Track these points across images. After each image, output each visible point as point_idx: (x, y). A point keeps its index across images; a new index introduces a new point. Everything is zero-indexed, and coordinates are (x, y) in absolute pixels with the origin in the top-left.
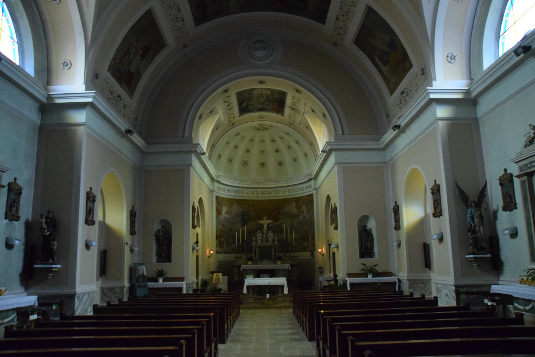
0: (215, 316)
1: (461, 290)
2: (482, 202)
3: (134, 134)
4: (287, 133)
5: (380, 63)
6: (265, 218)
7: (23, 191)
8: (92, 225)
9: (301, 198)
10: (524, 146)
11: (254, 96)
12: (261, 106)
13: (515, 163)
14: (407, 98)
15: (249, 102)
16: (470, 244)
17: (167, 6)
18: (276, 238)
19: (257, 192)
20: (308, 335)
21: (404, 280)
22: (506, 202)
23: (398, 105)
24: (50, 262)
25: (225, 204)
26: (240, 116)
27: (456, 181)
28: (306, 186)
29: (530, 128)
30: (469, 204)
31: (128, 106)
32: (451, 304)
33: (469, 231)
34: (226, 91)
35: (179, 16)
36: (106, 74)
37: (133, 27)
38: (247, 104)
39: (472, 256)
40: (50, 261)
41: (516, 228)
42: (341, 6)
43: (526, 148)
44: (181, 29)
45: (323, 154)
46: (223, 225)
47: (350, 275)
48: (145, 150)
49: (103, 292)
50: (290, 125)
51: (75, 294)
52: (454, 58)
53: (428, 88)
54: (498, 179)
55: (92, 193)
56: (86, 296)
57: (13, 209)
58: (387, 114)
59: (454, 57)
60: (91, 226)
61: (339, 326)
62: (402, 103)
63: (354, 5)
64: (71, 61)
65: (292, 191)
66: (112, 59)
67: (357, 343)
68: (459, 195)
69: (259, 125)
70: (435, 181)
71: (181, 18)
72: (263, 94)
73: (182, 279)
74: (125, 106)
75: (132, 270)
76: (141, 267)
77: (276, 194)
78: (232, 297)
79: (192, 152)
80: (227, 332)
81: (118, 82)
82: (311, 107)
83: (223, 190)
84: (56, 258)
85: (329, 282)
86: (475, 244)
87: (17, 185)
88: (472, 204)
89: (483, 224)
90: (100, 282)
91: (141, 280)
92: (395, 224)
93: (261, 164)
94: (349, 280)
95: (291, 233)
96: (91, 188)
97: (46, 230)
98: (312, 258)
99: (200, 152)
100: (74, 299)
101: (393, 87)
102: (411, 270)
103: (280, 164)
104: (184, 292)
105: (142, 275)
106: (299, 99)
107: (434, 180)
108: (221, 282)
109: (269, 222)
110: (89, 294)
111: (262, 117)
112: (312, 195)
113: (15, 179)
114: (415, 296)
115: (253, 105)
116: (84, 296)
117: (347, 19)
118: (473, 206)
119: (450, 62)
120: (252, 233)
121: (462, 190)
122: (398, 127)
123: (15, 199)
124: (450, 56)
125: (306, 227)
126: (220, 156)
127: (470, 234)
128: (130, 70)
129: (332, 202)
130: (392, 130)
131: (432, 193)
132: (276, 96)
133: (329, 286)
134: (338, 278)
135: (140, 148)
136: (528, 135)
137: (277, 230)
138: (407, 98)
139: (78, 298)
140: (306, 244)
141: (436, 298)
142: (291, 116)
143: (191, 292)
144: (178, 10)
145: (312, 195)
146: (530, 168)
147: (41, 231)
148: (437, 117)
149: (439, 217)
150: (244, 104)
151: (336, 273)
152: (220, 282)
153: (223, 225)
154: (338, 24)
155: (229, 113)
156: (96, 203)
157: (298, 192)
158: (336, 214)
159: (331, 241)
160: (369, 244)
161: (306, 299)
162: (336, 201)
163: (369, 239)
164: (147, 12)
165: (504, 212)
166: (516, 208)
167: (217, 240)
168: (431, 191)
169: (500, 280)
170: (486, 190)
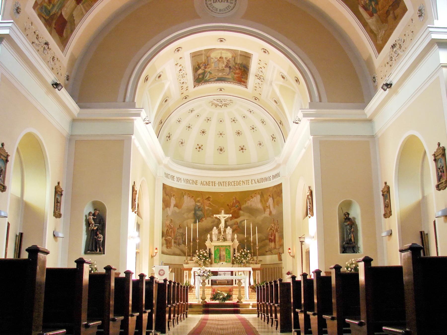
3: (62, 90)
11: (212, 60)
12: (220, 74)
15: (205, 68)
19: (213, 183)
23: (388, 63)
25: (174, 195)
34: (178, 50)
38: (203, 71)
46: (171, 220)
58: (374, 78)
62: (393, 59)
65: (256, 181)
70: (439, 144)
92: (385, 210)
93: (219, 150)
95: (254, 233)
98: (280, 262)
103: (242, 149)
107: (437, 143)
109: (227, 216)
111: (221, 90)
115: (211, 73)
125: (273, 225)
126: (169, 137)
128: (61, 14)
131: (435, 160)
140: (272, 245)
150: (200, 71)
153: (171, 220)
155: (182, 82)
156: (8, 164)
160: (352, 236)
163: (352, 230)
167: (164, 238)
168: (433, 158)
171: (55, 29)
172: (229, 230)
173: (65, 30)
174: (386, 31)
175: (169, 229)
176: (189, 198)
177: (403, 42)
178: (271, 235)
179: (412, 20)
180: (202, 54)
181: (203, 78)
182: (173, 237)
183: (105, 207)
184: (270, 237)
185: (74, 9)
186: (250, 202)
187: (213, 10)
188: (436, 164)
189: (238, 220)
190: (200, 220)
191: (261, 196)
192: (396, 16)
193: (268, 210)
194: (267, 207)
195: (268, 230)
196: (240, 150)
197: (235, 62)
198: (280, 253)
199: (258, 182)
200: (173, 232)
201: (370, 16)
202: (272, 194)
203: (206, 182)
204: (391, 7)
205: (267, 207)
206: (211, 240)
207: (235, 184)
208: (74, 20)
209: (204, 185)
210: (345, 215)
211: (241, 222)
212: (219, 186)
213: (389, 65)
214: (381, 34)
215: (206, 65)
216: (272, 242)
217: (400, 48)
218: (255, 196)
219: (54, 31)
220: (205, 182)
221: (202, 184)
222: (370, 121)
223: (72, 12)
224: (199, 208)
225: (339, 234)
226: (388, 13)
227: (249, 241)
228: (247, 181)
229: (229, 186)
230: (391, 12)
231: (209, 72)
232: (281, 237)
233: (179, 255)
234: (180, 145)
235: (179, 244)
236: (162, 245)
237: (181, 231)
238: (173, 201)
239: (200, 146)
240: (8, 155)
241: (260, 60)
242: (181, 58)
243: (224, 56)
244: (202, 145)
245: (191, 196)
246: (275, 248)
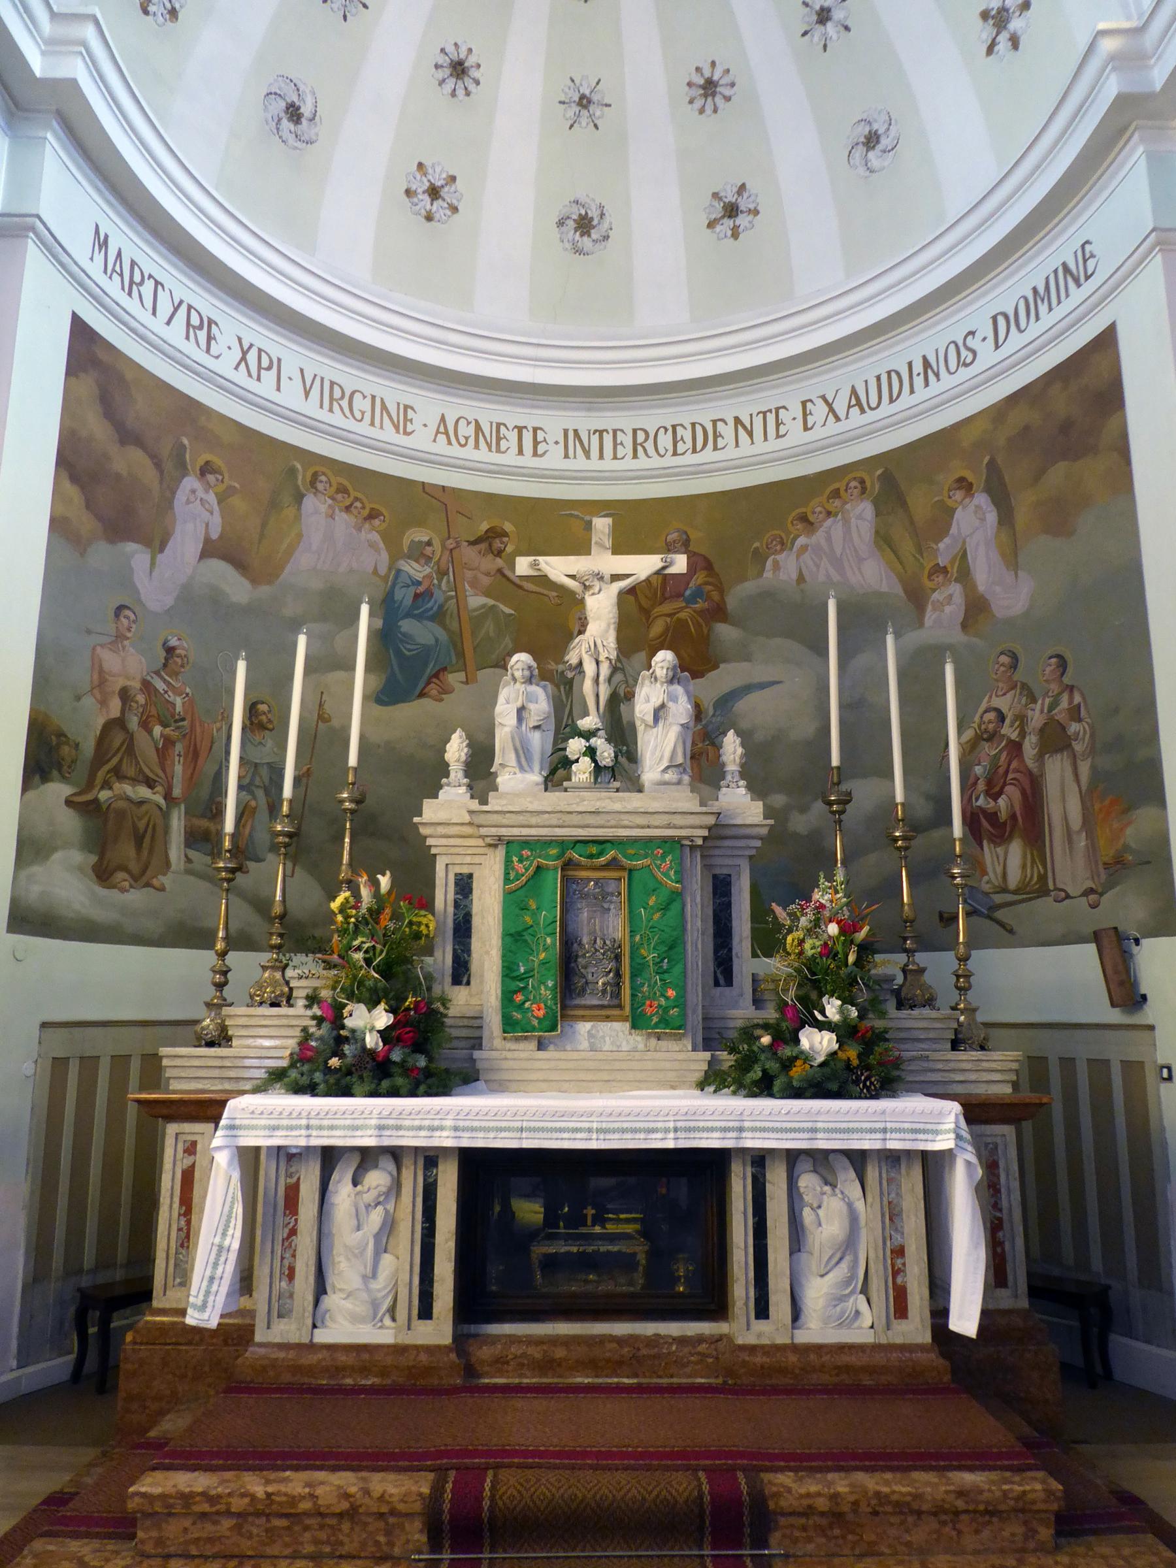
19: (528, 437)
46: (170, 651)
65: (840, 407)
77: (694, 451)
93: (571, 224)
109: (643, 566)
125: (1003, 703)
153: (170, 651)
175: (145, 725)
176: (342, 517)
178: (990, 783)
182: (177, 792)
186: (793, 557)
190: (428, 683)
193: (956, 590)
198: (1119, 936)
199: (855, 411)
200: (179, 747)
202: (992, 466)
203: (478, 428)
205: (944, 570)
207: (680, 444)
209: (462, 446)
212: (566, 456)
218: (829, 514)
220: (469, 423)
221: (447, 433)
224: (417, 596)
228: (771, 418)
229: (635, 456)
234: (280, 120)
245: (358, 504)
246: (1039, 888)
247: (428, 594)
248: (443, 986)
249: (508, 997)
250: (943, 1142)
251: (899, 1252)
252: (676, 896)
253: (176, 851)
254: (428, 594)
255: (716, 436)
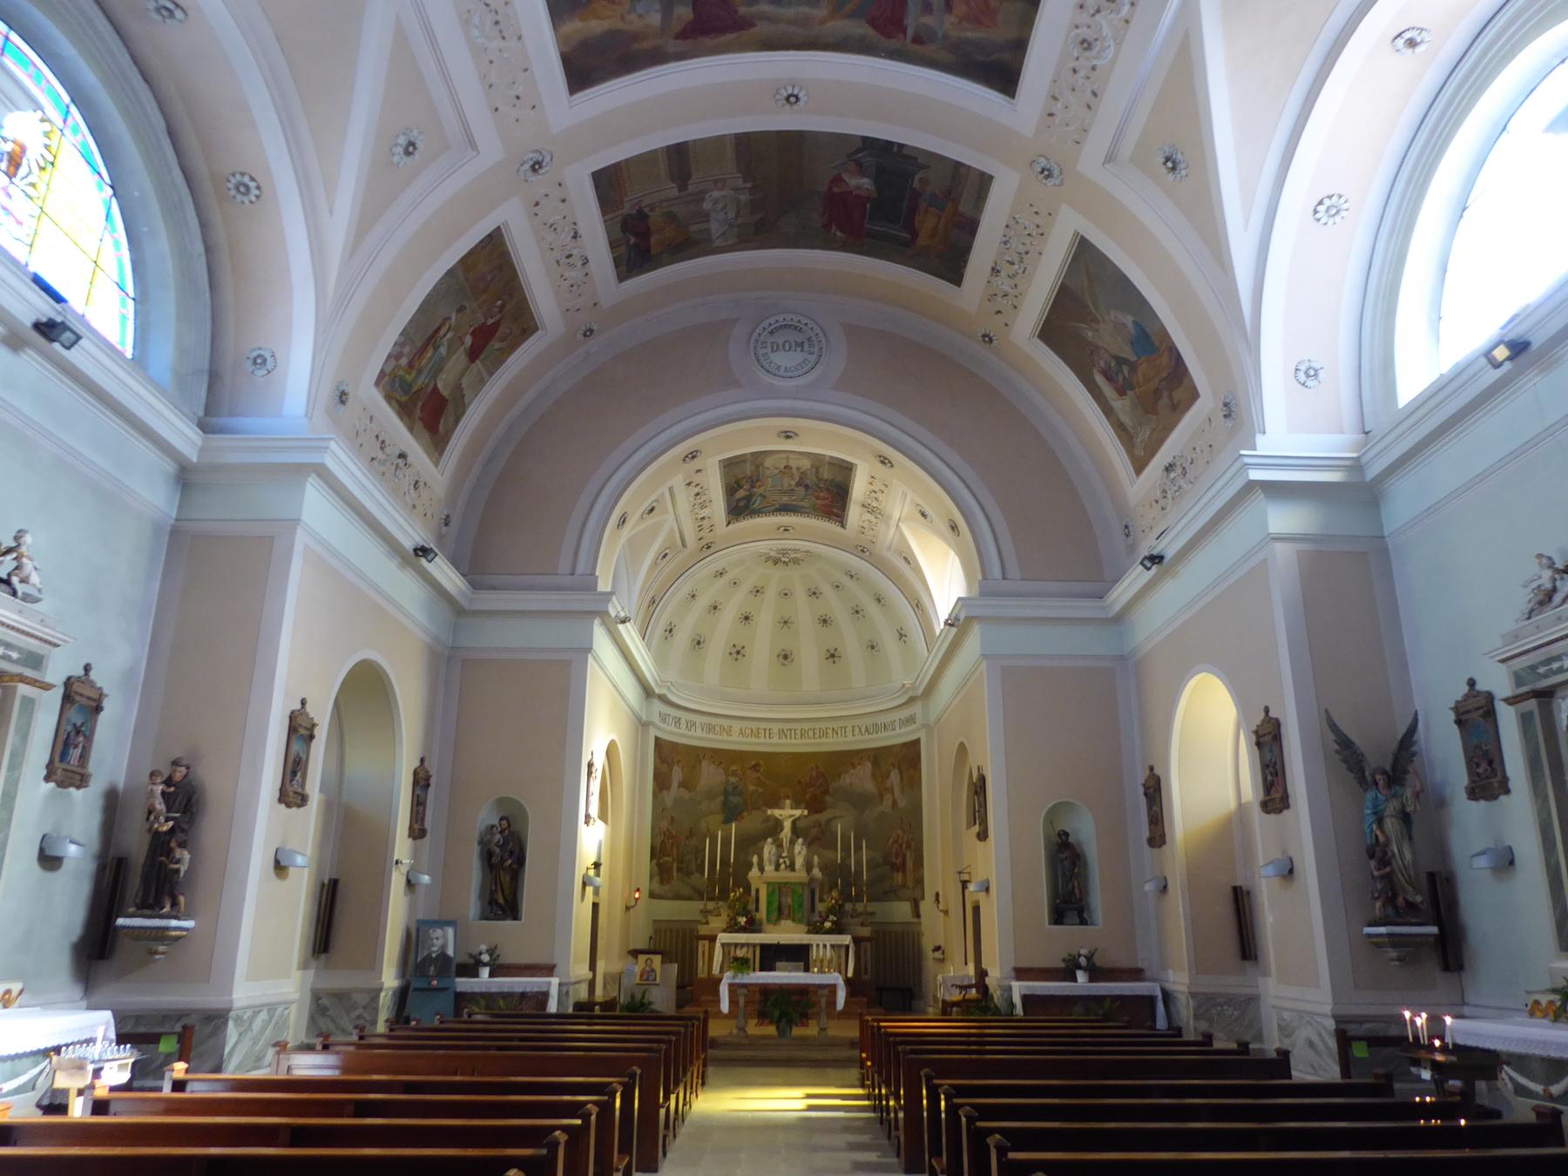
0: (677, 1042)
1: (1353, 1029)
2: (1406, 772)
4: (853, 573)
5: (1108, 391)
6: (788, 802)
7: (106, 703)
8: (299, 806)
9: (886, 750)
10: (1524, 614)
11: (768, 472)
12: (785, 499)
13: (1503, 661)
14: (1182, 483)
15: (753, 487)
16: (1376, 895)
17: (545, 224)
18: (816, 859)
20: (902, 1152)
21: (1182, 993)
22: (1478, 774)
23: (1157, 502)
24: (165, 910)
25: (678, 762)
26: (727, 526)
27: (1326, 711)
28: (900, 719)
29: (1540, 563)
30: (1369, 778)
31: (425, 484)
32: (1326, 1071)
33: (1371, 856)
34: (693, 455)
35: (574, 252)
36: (369, 395)
37: (450, 273)
38: (748, 493)
39: (1382, 930)
40: (163, 908)
41: (1510, 848)
42: (1005, 236)
43: (1530, 621)
44: (579, 286)
45: (948, 631)
47: (1022, 973)
48: (466, 605)
49: (318, 1005)
50: (861, 554)
51: (229, 1010)
52: (1316, 375)
53: (1243, 452)
54: (1452, 709)
55: (307, 714)
56: (263, 1015)
57: (71, 751)
58: (1126, 527)
59: (1316, 371)
60: (294, 809)
61: (1000, 1134)
62: (1169, 496)
63: (1042, 235)
64: (276, 354)
65: (863, 731)
66: (389, 357)
67: (1012, 1155)
68: (1337, 752)
69: (778, 551)
70: (1267, 710)
71: (582, 256)
72: (790, 468)
73: (549, 970)
74: (417, 482)
75: (413, 940)
76: (439, 932)
77: (820, 737)
78: (686, 1027)
79: (593, 614)
80: (665, 1137)
81: (401, 418)
82: (918, 505)
83: (676, 723)
84: (182, 899)
85: (964, 992)
86: (1390, 894)
87: (92, 684)
88: (1378, 777)
89: (1410, 838)
90: (311, 972)
91: (432, 968)
93: (781, 657)
94: (1018, 989)
95: (858, 848)
96: (303, 702)
97: (161, 818)
98: (915, 920)
99: (616, 616)
100: (225, 1023)
101: (1142, 454)
102: (1199, 965)
103: (833, 656)
104: (552, 1007)
105: (437, 956)
106: (887, 483)
107: (1263, 708)
108: (658, 981)
109: (797, 813)
110: (271, 1008)
111: (788, 530)
112: (917, 743)
113: (87, 668)
114: (1217, 1045)
115: (765, 497)
116: (256, 1014)
117: (1020, 271)
118: (1381, 783)
119: (1303, 384)
120: (750, 844)
121: (1345, 736)
122: (1157, 561)
123: (82, 725)
124: (1303, 368)
125: (900, 832)
126: (671, 631)
127: (1373, 863)
128: (435, 387)
129: (973, 761)
130: (1141, 567)
132: (826, 474)
133: (964, 1004)
134: (988, 980)
135: (457, 603)
136: (1535, 585)
137: (817, 837)
138: (1182, 483)
139: (238, 1019)
140: (898, 877)
141: (1284, 1055)
142: (863, 527)
143: (570, 1011)
144: (572, 234)
145: (917, 743)
146: (1546, 676)
147: (148, 819)
148: (1271, 532)
149: (1281, 811)
150: (741, 493)
151: (984, 966)
152: (655, 980)
153: (672, 818)
154: (995, 285)
157: (879, 735)
158: (982, 798)
159: (969, 873)
161: (898, 1039)
162: (989, 759)
164: (490, 236)
165: (1473, 803)
166: (1507, 791)
167: (654, 862)
169: (1468, 1004)
170: (1415, 738)
171: (421, 419)
172: (799, 847)
173: (442, 421)
174: (1154, 430)
175: (668, 840)
177: (1191, 463)
179: (1210, 420)
180: (745, 461)
181: (747, 506)
183: (525, 812)
184: (894, 860)
185: (462, 375)
187: (770, 370)
188: (1260, 752)
189: (822, 817)
191: (873, 764)
192: (1175, 402)
194: (886, 789)
195: (890, 843)
196: (827, 658)
197: (817, 477)
201: (1118, 393)
204: (1164, 383)
206: (761, 869)
208: (463, 396)
210: (1059, 835)
211: (829, 821)
213: (1159, 506)
214: (1144, 434)
215: (754, 481)
216: (898, 871)
217: (1184, 475)
219: (419, 425)
222: (1119, 619)
223: (460, 379)
225: (1045, 855)
226: (1157, 393)
227: (845, 866)
230: (1165, 394)
231: (761, 495)
232: (919, 863)
233: (689, 898)
235: (689, 874)
236: (651, 877)
237: (694, 842)
238: (677, 775)
239: (738, 648)
240: (314, 725)
241: (873, 477)
242: (698, 471)
243: (793, 463)
244: (743, 647)
247: (737, 787)
248: (754, 913)
249: (768, 916)
250: (847, 943)
251: (840, 963)
252: (801, 895)
253: (675, 874)
254: (737, 787)
255: (827, 734)
